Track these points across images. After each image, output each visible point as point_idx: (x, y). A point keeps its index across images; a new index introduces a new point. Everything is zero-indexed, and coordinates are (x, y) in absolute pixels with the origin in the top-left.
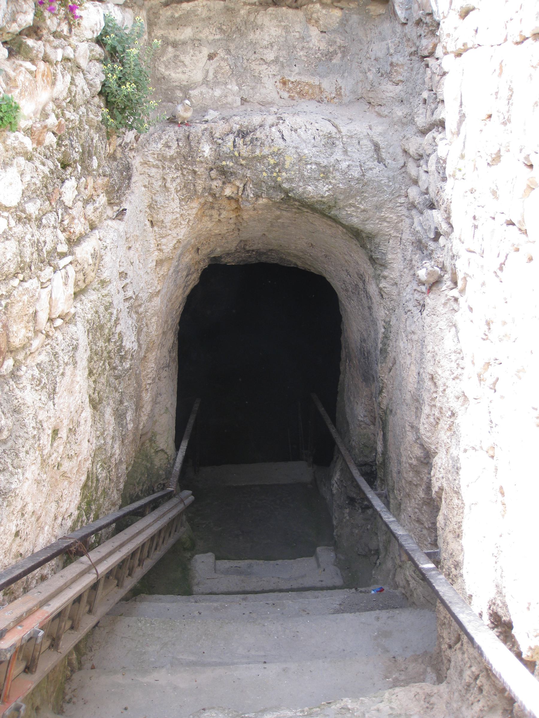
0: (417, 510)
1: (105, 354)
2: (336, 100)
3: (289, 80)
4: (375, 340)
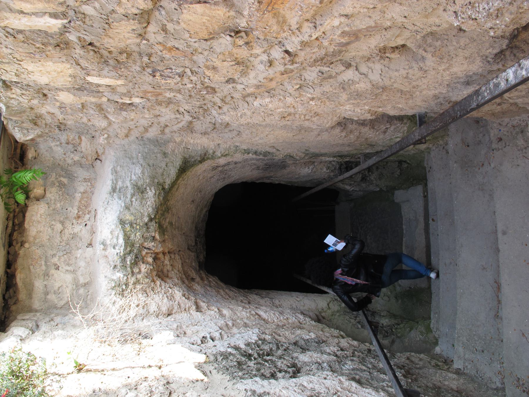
0: (377, 133)
3: (77, 214)
4: (258, 160)
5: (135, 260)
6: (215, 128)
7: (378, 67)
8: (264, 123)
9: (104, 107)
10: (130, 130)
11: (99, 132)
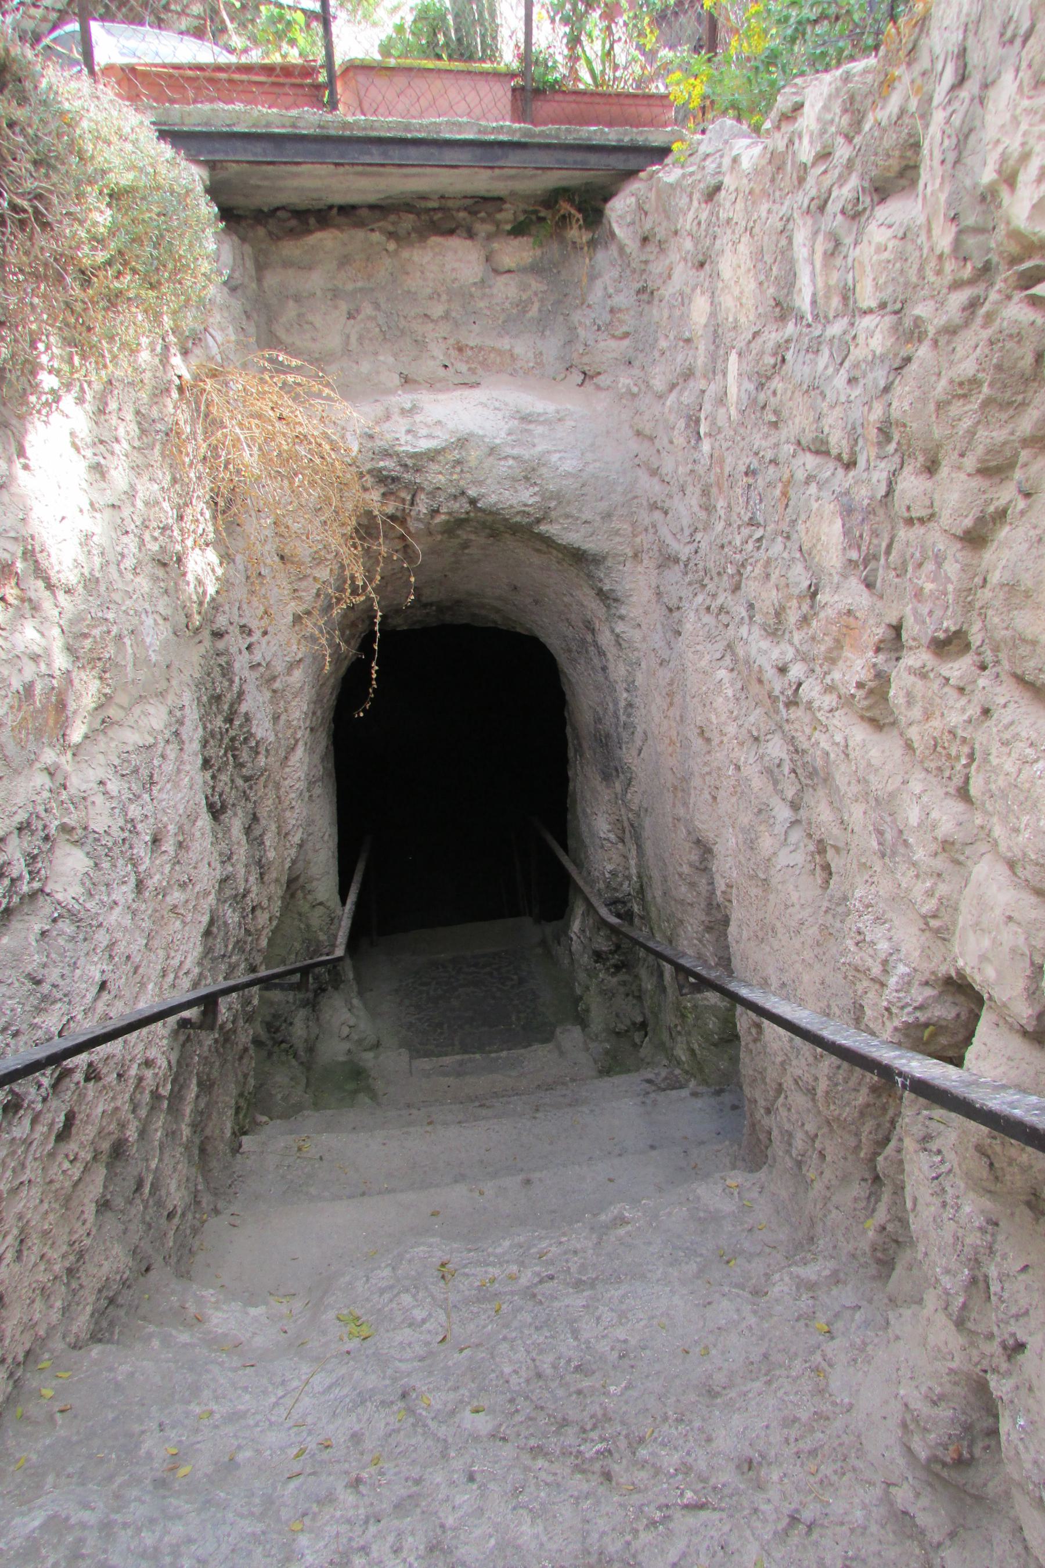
1: (226, 740)
2: (535, 371)
5: (387, 477)
6: (671, 610)
7: (799, 858)
8: (688, 699)
9: (691, 383)
10: (652, 439)
11: (642, 374)
